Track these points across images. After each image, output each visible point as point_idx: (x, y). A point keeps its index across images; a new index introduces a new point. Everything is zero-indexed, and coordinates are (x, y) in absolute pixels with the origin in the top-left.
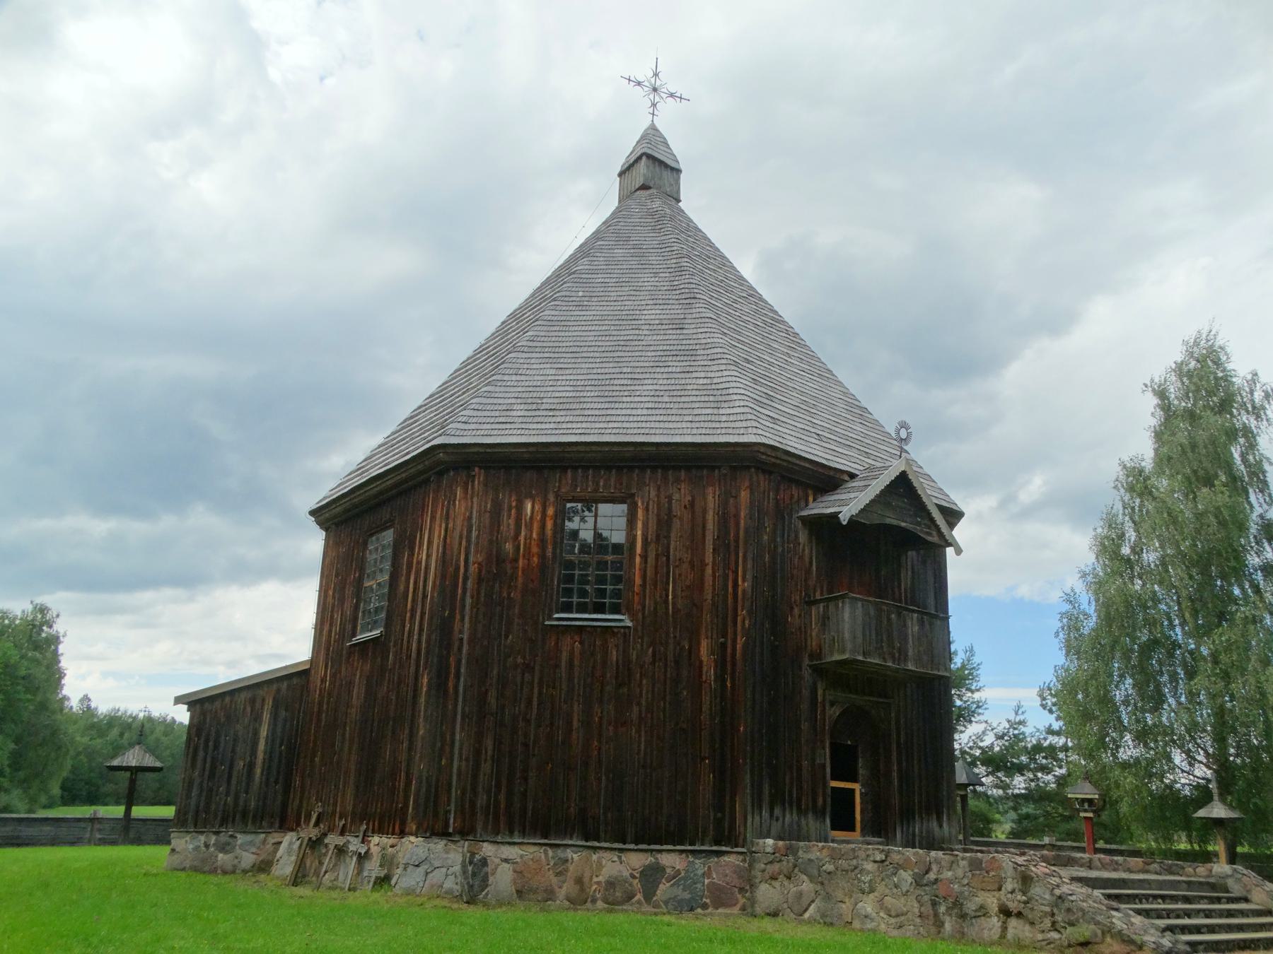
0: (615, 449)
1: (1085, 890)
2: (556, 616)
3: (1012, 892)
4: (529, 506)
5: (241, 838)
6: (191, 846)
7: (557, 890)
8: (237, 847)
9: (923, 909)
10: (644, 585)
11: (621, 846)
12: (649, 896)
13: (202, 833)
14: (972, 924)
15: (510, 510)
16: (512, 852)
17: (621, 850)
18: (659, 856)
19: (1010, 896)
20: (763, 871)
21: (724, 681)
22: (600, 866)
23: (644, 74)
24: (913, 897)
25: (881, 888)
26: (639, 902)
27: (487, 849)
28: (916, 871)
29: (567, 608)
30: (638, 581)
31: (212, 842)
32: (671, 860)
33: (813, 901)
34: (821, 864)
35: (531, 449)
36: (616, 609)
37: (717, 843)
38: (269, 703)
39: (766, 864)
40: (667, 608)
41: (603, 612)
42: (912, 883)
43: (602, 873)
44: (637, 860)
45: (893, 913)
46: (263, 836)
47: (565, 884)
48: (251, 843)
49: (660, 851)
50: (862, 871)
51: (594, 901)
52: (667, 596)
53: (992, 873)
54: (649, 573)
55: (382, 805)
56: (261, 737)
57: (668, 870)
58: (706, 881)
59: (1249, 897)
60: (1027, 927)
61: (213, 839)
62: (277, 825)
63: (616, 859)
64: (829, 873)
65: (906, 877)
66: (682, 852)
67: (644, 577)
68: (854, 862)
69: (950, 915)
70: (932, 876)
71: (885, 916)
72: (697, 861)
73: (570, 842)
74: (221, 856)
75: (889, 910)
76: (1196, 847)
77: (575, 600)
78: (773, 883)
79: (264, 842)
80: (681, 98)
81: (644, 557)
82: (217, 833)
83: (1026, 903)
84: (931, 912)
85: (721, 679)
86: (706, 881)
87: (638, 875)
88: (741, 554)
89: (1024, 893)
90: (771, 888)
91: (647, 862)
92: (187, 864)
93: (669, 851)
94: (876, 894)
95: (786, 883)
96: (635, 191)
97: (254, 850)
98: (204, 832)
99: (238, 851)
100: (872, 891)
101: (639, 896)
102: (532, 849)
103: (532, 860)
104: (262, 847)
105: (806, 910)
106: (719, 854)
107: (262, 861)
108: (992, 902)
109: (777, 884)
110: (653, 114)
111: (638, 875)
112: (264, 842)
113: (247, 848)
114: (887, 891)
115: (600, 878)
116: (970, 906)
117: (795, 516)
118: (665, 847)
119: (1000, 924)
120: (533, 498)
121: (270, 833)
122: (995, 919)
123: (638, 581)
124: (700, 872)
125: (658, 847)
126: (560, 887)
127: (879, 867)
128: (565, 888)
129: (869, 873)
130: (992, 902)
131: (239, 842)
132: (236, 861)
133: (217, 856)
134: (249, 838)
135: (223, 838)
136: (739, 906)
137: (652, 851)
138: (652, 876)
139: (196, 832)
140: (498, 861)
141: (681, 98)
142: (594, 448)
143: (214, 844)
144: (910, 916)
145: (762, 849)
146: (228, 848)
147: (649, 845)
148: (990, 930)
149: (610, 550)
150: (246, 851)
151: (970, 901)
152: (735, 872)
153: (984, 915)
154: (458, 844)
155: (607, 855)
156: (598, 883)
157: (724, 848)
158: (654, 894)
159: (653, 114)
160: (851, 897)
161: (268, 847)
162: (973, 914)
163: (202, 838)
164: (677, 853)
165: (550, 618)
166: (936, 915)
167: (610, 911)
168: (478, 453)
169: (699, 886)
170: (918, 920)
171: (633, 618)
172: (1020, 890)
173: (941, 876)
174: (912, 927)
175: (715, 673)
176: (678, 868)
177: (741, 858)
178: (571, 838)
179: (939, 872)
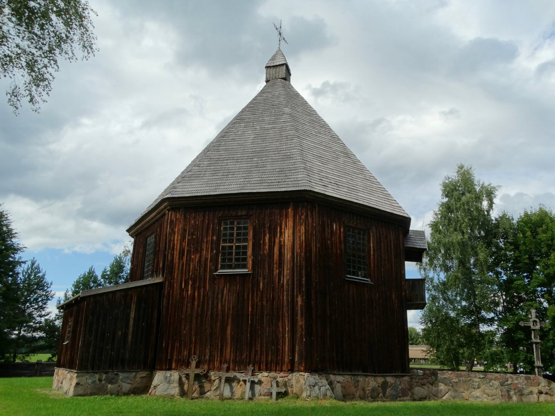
0: (369, 209)
3: (544, 386)
4: (335, 225)
5: (121, 375)
6: (90, 381)
7: (355, 393)
8: (119, 380)
9: (502, 393)
10: (374, 267)
11: (375, 374)
12: (384, 394)
13: (97, 373)
14: (526, 397)
15: (328, 227)
16: (340, 378)
18: (386, 378)
19: (543, 388)
22: (369, 383)
24: (499, 390)
25: (483, 387)
26: (381, 397)
28: (501, 381)
30: (372, 265)
31: (104, 378)
32: (390, 380)
33: (447, 393)
34: (451, 379)
35: (340, 201)
38: (135, 299)
39: (419, 380)
42: (499, 385)
43: (370, 386)
44: (380, 380)
45: (490, 395)
46: (134, 374)
47: (358, 391)
48: (128, 378)
49: (386, 376)
50: (473, 382)
51: (368, 398)
53: (535, 381)
54: (376, 263)
55: (267, 356)
56: (131, 318)
57: (389, 383)
58: (400, 387)
60: (549, 397)
61: (104, 376)
62: (142, 367)
63: (373, 380)
64: (456, 382)
65: (497, 383)
66: (392, 376)
67: (374, 264)
68: (469, 378)
69: (516, 395)
70: (509, 382)
71: (486, 396)
72: (397, 380)
74: (109, 386)
75: (489, 394)
77: (351, 270)
78: (423, 387)
79: (135, 377)
81: (374, 255)
82: (106, 373)
83: (550, 389)
84: (507, 394)
86: (400, 387)
87: (380, 386)
89: (549, 387)
90: (422, 388)
91: (383, 381)
92: (89, 391)
94: (481, 389)
96: (281, 78)
97: (129, 381)
98: (98, 372)
99: (120, 382)
100: (479, 388)
101: (381, 395)
102: (347, 377)
103: (347, 381)
104: (133, 379)
105: (444, 396)
106: (403, 376)
107: (135, 388)
108: (535, 390)
111: (380, 386)
112: (135, 377)
113: (125, 381)
114: (486, 388)
115: (369, 388)
116: (526, 392)
119: (537, 396)
120: (335, 222)
121: (138, 372)
122: (535, 395)
123: (372, 265)
125: (385, 374)
126: (357, 393)
127: (481, 380)
128: (358, 393)
129: (476, 382)
130: (535, 390)
131: (121, 377)
132: (119, 388)
133: (107, 386)
134: (126, 375)
135: (110, 375)
136: (409, 396)
138: (385, 385)
139: (93, 372)
140: (336, 382)
142: (361, 207)
143: (105, 380)
144: (498, 396)
145: (416, 374)
146: (114, 381)
147: (383, 373)
148: (533, 398)
150: (124, 382)
151: (526, 390)
153: (531, 394)
154: (322, 375)
156: (369, 390)
157: (405, 374)
158: (386, 393)
160: (468, 390)
161: (137, 379)
162: (527, 394)
163: (97, 376)
164: (390, 377)
166: (509, 395)
167: (374, 401)
168: (321, 198)
169: (398, 389)
170: (501, 397)
172: (547, 386)
173: (513, 382)
174: (499, 399)
176: (392, 382)
178: (359, 372)
179: (512, 381)
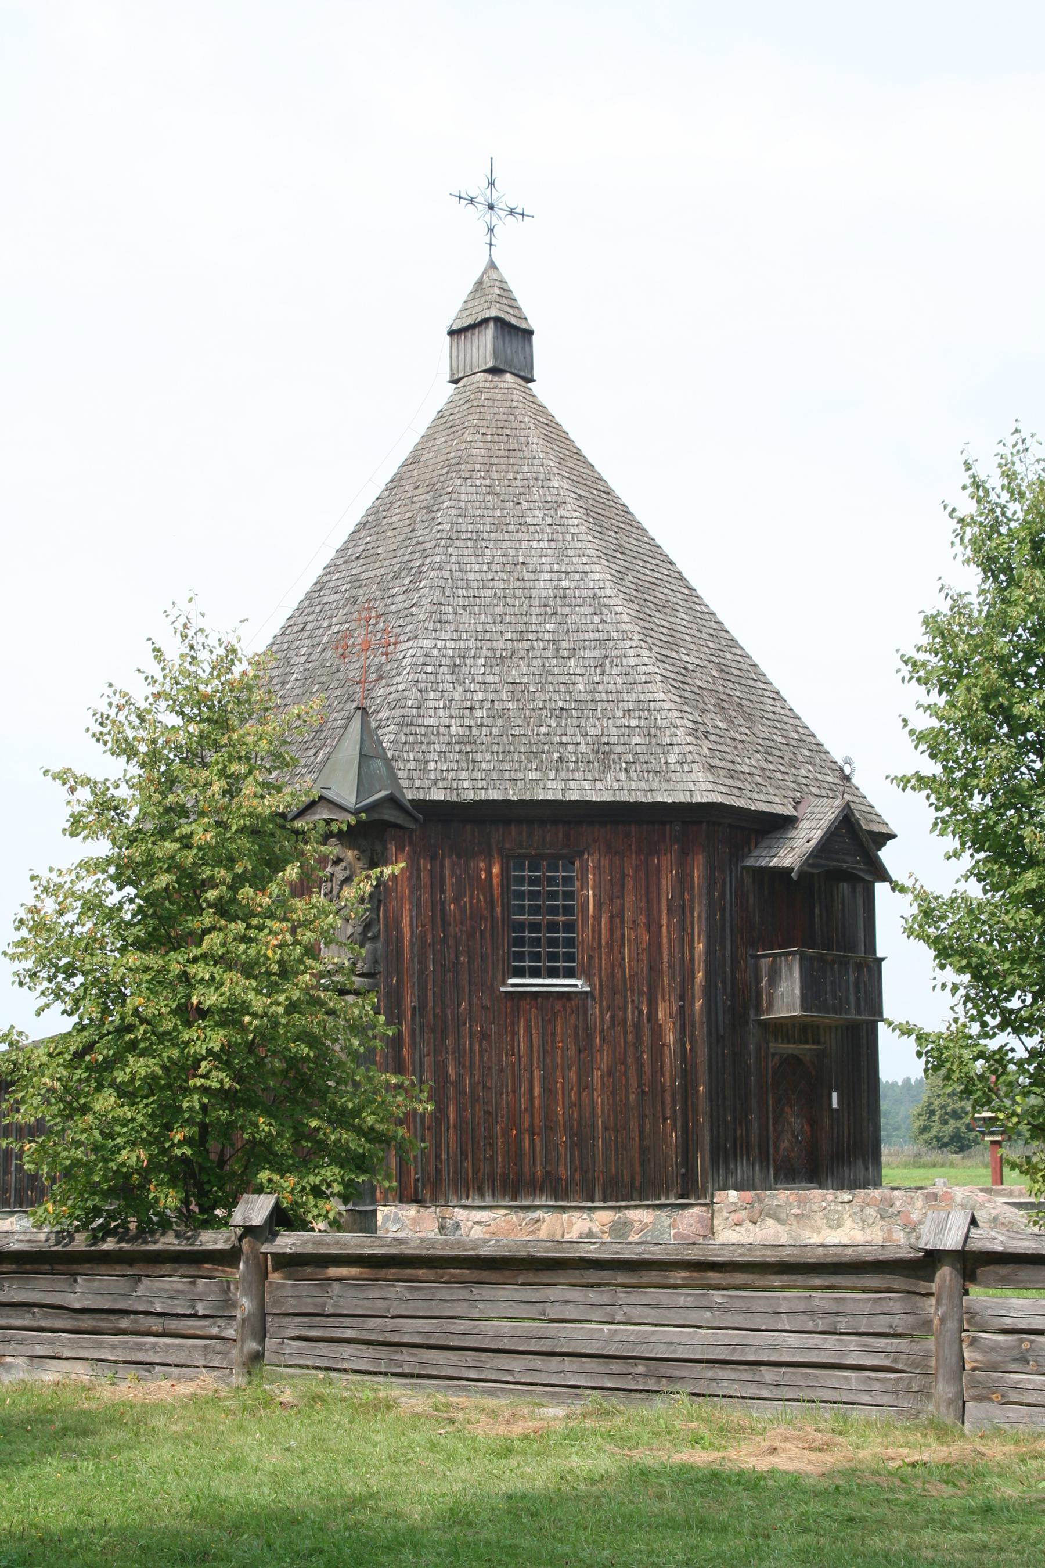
1: (1015, 1210)
2: (511, 981)
11: (589, 1204)
17: (590, 1208)
18: (627, 1212)
20: (727, 1219)
21: (683, 1044)
22: (571, 1224)
23: (476, 187)
27: (459, 1214)
29: (519, 973)
36: (570, 973)
37: (682, 1197)
40: (624, 972)
41: (557, 976)
49: (627, 1207)
52: (623, 959)
57: (636, 1224)
59: (455, 386)
66: (648, 1207)
73: (503, 1204)
76: (536, 1410)
80: (523, 215)
85: (681, 1041)
86: (673, 1232)
88: (696, 914)
93: (636, 1207)
95: (751, 1227)
109: (742, 1229)
110: (491, 245)
117: (740, 864)
118: (633, 1203)
124: (666, 1224)
137: (620, 1207)
141: (523, 215)
149: (561, 911)
152: (699, 1222)
155: (577, 1214)
159: (491, 245)
165: (504, 984)
169: (666, 1236)
171: (589, 979)
175: (674, 1038)
177: (704, 1208)
